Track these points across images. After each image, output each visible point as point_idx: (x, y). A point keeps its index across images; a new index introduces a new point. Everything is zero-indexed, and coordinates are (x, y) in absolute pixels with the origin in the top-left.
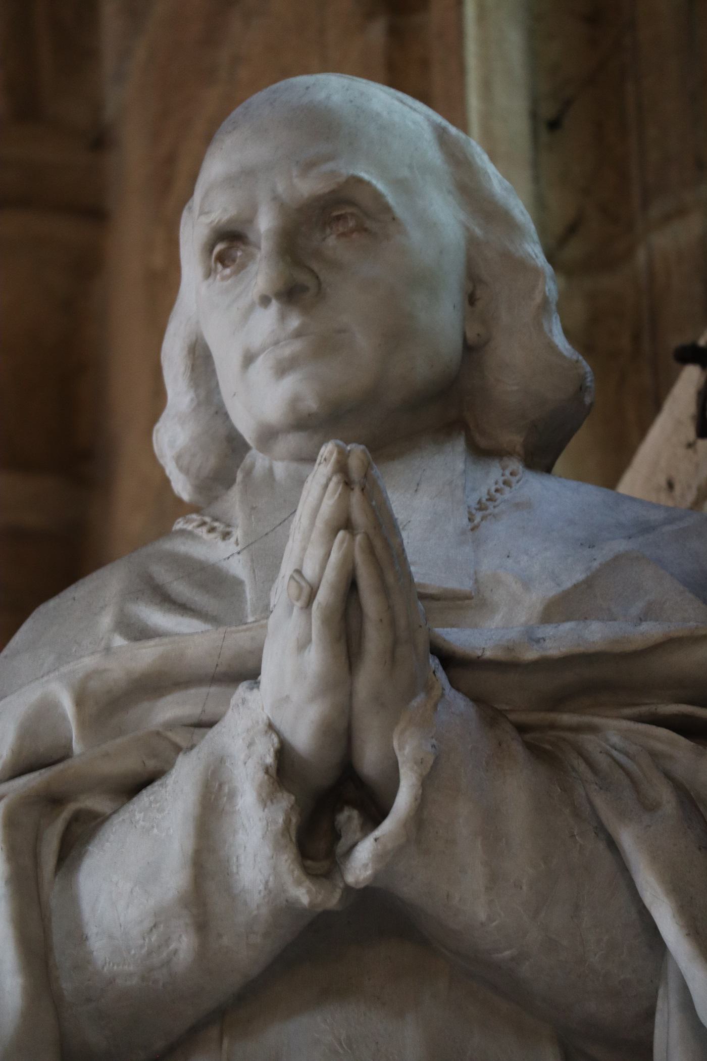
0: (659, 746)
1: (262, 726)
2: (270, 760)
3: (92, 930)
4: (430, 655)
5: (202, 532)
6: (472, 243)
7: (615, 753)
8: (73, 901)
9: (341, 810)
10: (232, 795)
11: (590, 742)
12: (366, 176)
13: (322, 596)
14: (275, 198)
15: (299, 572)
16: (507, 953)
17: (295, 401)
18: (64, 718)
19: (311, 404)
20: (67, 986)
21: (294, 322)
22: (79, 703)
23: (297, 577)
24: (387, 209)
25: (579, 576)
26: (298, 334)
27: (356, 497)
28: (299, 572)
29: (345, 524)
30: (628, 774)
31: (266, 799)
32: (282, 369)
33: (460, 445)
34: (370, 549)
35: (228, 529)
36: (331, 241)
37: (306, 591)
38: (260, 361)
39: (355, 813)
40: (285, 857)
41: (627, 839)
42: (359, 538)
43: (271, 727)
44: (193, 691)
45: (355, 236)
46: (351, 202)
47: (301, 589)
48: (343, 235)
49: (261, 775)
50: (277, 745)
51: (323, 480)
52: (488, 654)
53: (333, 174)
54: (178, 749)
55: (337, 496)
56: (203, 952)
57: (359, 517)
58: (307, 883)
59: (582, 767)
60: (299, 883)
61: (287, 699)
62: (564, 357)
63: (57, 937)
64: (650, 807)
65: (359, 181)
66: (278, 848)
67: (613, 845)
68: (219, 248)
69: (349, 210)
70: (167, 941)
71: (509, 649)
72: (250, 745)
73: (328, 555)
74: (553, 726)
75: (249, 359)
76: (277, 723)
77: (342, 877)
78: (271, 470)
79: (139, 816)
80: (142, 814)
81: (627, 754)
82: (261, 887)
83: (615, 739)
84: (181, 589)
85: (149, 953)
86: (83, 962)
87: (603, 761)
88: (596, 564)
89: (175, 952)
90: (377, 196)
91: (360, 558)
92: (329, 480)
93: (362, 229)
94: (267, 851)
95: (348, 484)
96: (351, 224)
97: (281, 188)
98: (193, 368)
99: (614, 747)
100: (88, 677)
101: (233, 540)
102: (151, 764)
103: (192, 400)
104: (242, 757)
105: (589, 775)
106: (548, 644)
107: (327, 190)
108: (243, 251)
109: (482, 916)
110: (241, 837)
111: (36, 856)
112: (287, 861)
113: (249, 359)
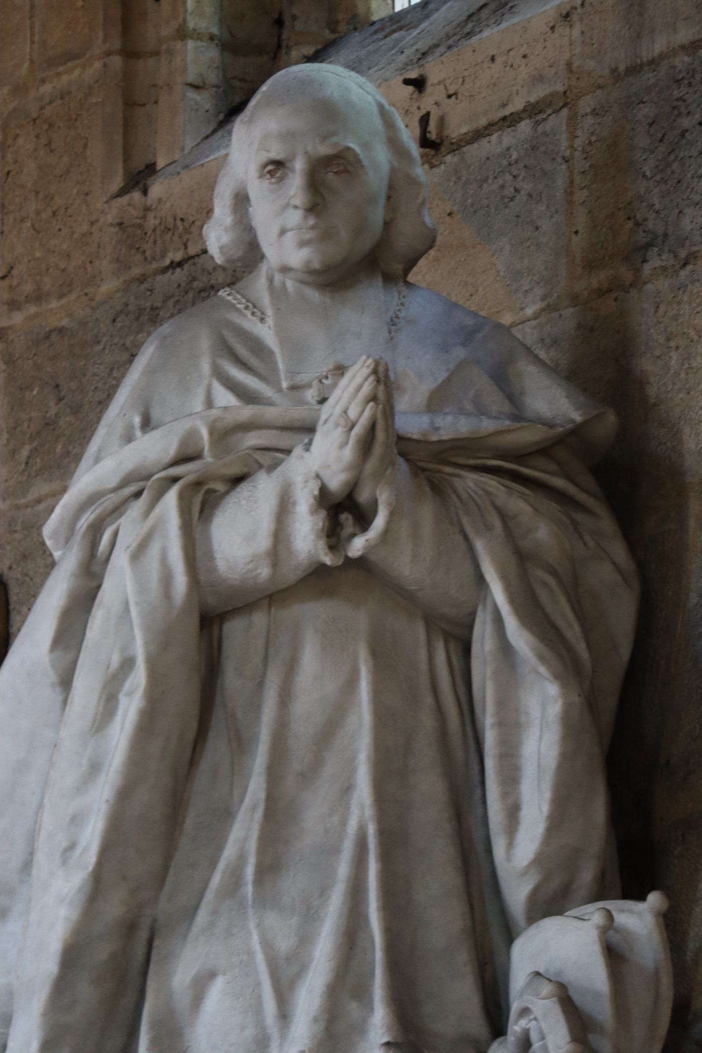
0: (491, 489)
1: (313, 475)
2: (316, 492)
3: (218, 556)
4: (398, 456)
5: (248, 313)
6: (393, 170)
7: (469, 490)
8: (208, 538)
9: (342, 512)
10: (294, 504)
11: (457, 482)
12: (351, 145)
13: (358, 430)
14: (306, 153)
15: (345, 412)
16: (414, 587)
17: (308, 262)
18: (201, 438)
19: (317, 265)
20: (202, 578)
21: (311, 221)
22: (211, 433)
23: (344, 415)
24: (359, 161)
25: (444, 375)
26: (313, 228)
27: (381, 388)
28: (345, 412)
29: (373, 398)
30: (477, 505)
31: (313, 512)
32: (302, 244)
33: (379, 282)
34: (384, 413)
35: (263, 316)
36: (330, 176)
37: (350, 425)
38: (290, 234)
39: (350, 517)
40: (321, 542)
41: (480, 546)
42: (380, 406)
43: (318, 476)
44: (264, 431)
45: (343, 175)
46: (342, 158)
47: (347, 423)
48: (336, 173)
49: (312, 501)
50: (320, 486)
51: (365, 375)
52: (415, 437)
53: (336, 144)
54: (261, 466)
55: (372, 386)
56: (273, 576)
57: (381, 395)
58: (330, 555)
59: (453, 496)
60: (326, 555)
61: (329, 466)
62: (427, 227)
63: (199, 554)
64: (489, 528)
65: (348, 149)
66: (318, 537)
67: (471, 549)
68: (270, 168)
69: (342, 161)
70: (257, 569)
71: (425, 435)
72: (306, 482)
73: (363, 411)
74: (440, 472)
75: (283, 232)
76: (322, 474)
77: (345, 551)
78: (284, 284)
79: (243, 502)
80: (245, 502)
81: (477, 494)
82: (307, 552)
83: (471, 484)
84: (241, 350)
85: (246, 572)
86: (212, 569)
87: (464, 496)
88: (451, 366)
89: (260, 573)
90: (356, 155)
91: (379, 416)
92: (366, 379)
93: (346, 171)
94: (312, 537)
95: (378, 381)
96: (342, 168)
97: (309, 148)
98: (236, 204)
99: (470, 487)
100: (215, 421)
101: (267, 325)
102: (245, 470)
103: (232, 220)
104: (301, 486)
105: (458, 504)
106: (442, 432)
107: (333, 153)
108: (283, 171)
109: (407, 573)
110: (297, 525)
111: (190, 512)
112: (322, 544)
113: (283, 232)
